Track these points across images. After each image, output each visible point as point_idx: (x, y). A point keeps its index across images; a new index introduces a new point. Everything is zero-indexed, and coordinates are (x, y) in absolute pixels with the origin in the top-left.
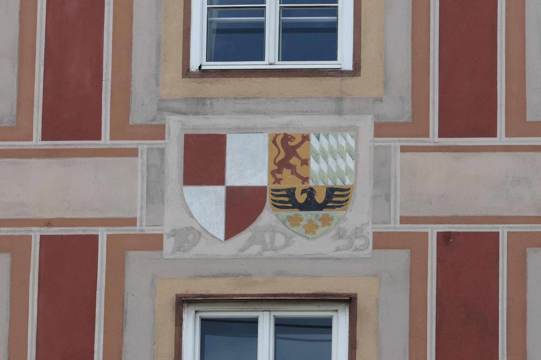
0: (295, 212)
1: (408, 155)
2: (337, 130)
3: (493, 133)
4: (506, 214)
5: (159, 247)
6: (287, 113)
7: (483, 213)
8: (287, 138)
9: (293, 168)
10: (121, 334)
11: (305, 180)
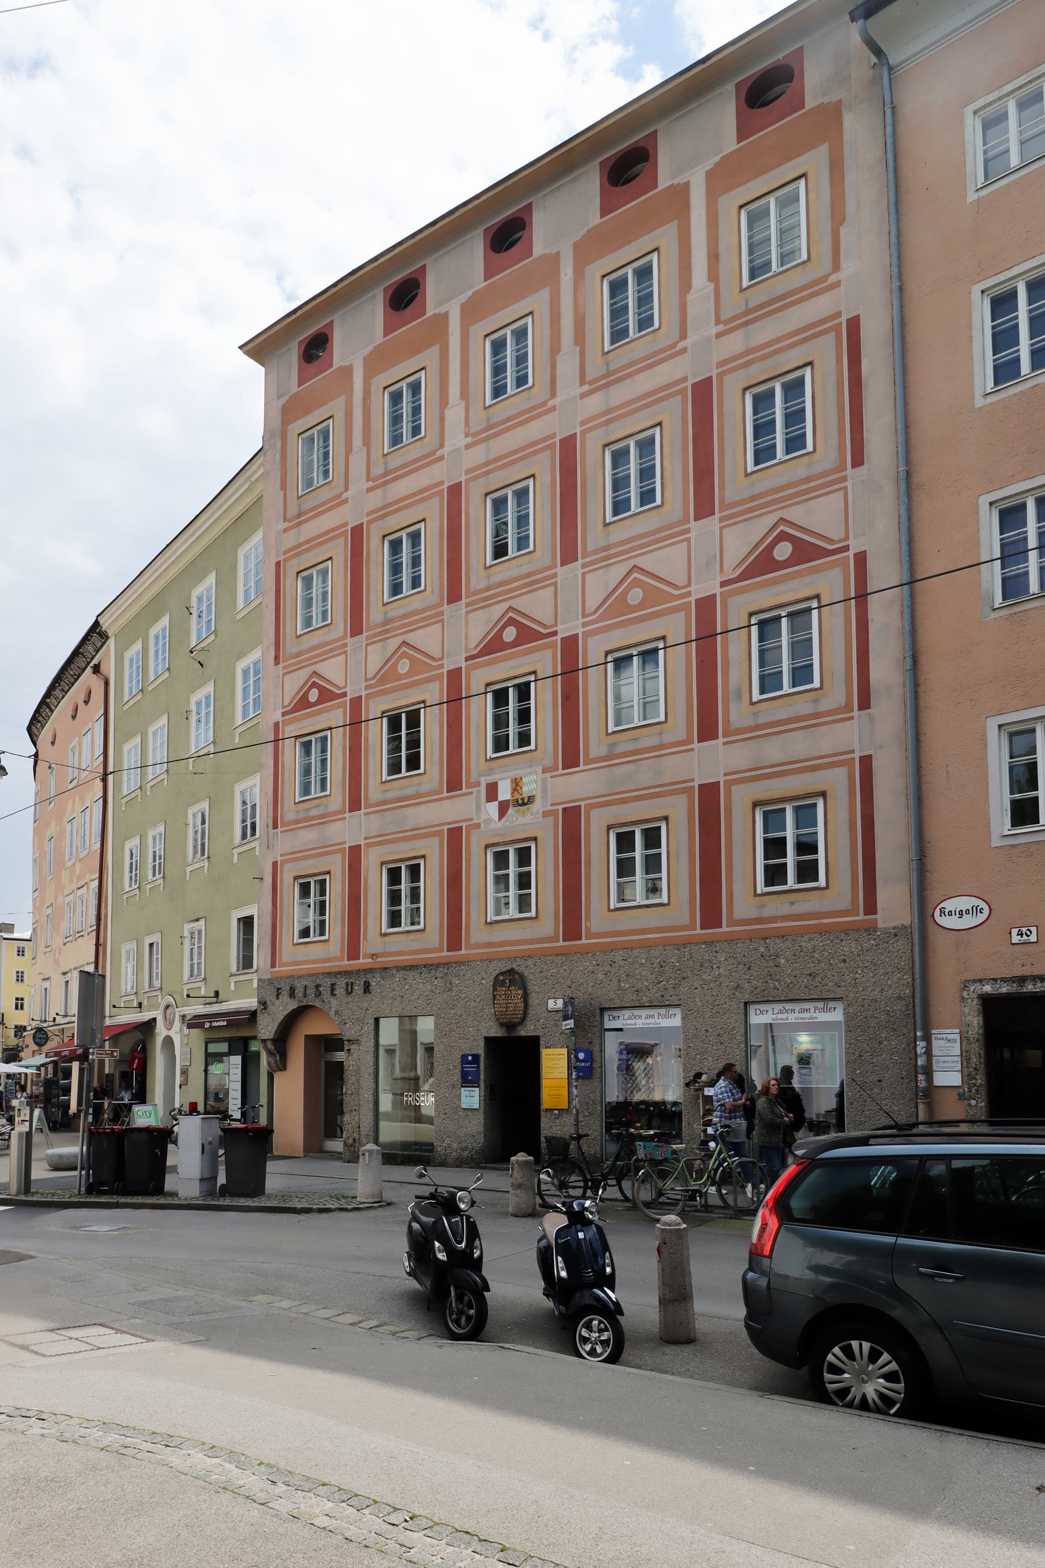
0: (519, 807)
1: (552, 779)
2: (531, 773)
3: (578, 765)
4: (685, 779)
5: (480, 828)
6: (516, 769)
7: (775, 762)
8: (516, 779)
9: (517, 791)
10: (470, 861)
11: (521, 794)
